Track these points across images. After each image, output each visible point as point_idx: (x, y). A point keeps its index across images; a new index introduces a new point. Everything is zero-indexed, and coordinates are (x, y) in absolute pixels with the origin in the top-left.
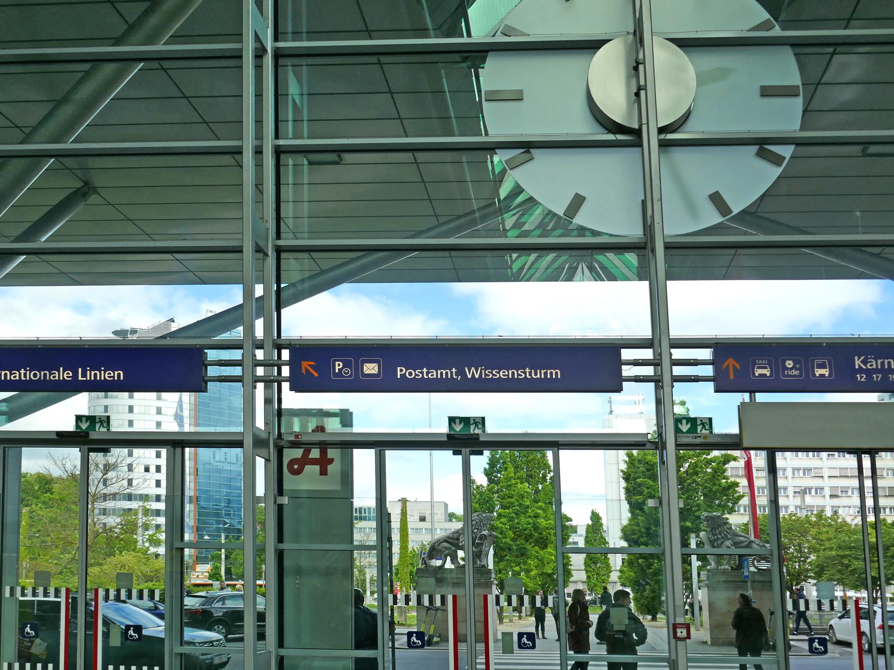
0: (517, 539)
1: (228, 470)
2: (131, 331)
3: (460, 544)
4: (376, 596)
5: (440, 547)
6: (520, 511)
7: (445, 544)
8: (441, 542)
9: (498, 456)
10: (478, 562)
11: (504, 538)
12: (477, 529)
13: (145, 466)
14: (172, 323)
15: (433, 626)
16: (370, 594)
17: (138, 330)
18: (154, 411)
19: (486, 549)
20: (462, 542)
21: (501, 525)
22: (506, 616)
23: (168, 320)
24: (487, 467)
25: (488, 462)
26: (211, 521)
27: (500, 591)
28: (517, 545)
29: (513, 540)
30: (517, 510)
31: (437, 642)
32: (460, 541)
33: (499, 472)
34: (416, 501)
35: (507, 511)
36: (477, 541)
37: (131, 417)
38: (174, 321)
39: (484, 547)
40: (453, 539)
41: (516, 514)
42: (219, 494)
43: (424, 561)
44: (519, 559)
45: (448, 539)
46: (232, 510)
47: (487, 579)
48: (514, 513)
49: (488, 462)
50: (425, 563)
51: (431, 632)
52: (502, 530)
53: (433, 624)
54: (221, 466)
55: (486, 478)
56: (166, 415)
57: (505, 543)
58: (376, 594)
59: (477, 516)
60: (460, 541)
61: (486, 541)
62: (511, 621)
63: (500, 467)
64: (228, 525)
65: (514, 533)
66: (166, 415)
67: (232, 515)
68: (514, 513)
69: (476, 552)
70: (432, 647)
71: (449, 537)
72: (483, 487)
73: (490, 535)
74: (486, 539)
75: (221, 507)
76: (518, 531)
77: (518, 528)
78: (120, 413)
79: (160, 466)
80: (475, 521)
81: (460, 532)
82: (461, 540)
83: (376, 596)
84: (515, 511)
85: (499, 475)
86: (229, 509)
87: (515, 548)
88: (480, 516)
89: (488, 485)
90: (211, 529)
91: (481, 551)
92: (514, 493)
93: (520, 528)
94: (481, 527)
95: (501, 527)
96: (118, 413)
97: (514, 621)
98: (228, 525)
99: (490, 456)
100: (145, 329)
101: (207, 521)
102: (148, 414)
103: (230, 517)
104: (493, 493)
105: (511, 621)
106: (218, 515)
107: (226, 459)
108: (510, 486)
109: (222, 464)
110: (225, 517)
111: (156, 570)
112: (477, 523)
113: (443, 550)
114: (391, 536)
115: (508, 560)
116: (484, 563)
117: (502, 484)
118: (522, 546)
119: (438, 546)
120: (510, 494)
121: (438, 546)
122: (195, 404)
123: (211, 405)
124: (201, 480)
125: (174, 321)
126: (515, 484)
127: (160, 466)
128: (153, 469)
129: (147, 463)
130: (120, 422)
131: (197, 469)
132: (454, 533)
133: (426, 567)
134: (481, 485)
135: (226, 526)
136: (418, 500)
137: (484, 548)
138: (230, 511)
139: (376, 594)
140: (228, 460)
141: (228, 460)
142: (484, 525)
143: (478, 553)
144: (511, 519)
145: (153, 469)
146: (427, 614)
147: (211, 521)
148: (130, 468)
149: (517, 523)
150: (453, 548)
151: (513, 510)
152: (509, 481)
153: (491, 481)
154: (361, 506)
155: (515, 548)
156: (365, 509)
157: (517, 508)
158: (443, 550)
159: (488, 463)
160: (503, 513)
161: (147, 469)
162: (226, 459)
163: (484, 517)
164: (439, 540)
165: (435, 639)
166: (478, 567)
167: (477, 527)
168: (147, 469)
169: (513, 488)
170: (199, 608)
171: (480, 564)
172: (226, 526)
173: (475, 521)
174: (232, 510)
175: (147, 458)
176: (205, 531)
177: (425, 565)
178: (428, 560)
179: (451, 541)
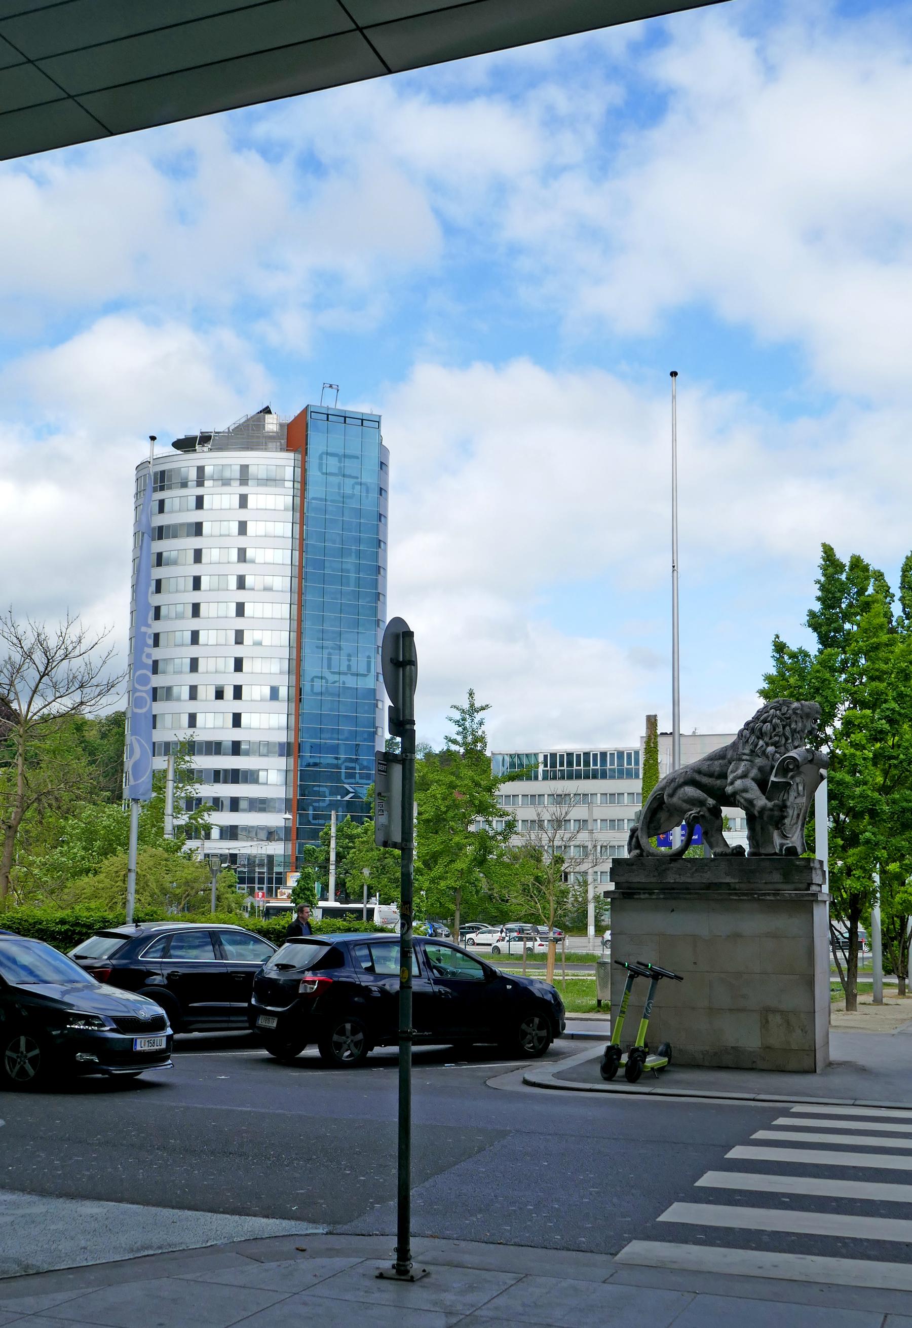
0: (893, 787)
1: (354, 688)
2: (200, 437)
3: (729, 789)
4: (608, 935)
5: (675, 800)
6: (900, 714)
7: (690, 791)
8: (681, 786)
9: (843, 577)
10: (777, 840)
11: (858, 783)
12: (775, 744)
13: (216, 688)
14: (267, 416)
15: (644, 1024)
16: (596, 931)
17: (212, 434)
18: (233, 582)
19: (798, 800)
20: (732, 783)
21: (852, 751)
22: (865, 984)
23: (261, 412)
24: (817, 607)
25: (819, 594)
26: (322, 789)
27: (848, 924)
28: (894, 802)
29: (884, 790)
30: (893, 710)
31: (661, 1070)
32: (729, 780)
33: (847, 617)
34: (694, 735)
35: (868, 712)
36: (773, 778)
37: (195, 597)
38: (269, 412)
39: (793, 794)
40: (710, 775)
41: (891, 721)
42: (335, 736)
43: (634, 840)
44: (898, 838)
45: (698, 777)
46: (358, 767)
47: (800, 886)
48: (886, 718)
49: (819, 594)
50: (638, 846)
51: (640, 1043)
52: (857, 765)
53: (645, 1017)
54: (341, 682)
55: (815, 634)
56: (253, 589)
57: (861, 796)
58: (608, 932)
59: (776, 708)
60: (729, 780)
61: (798, 779)
62: (878, 1001)
63: (850, 605)
64: (351, 795)
65: (886, 773)
66: (253, 589)
67: (357, 776)
68: (886, 718)
69: (771, 810)
70: (643, 1084)
71: (699, 772)
72: (806, 655)
73: (811, 761)
74: (799, 773)
75: (340, 762)
76: (896, 766)
77: (896, 758)
78: (180, 592)
79: (241, 686)
80: (771, 722)
81: (730, 754)
82: (730, 777)
83: (608, 935)
84: (888, 713)
85: (847, 626)
86: (353, 765)
87: (886, 808)
88: (784, 709)
89: (821, 652)
90: (321, 804)
91: (783, 807)
92: (884, 667)
93: (902, 756)
94: (787, 739)
95: (853, 755)
96: (177, 591)
97: (885, 1000)
98: (351, 795)
99: (823, 579)
100: (223, 432)
101: (315, 789)
102: (223, 590)
103: (352, 781)
104: (833, 670)
105: (878, 1001)
106: (336, 777)
107: (349, 667)
108: (876, 648)
109: (343, 678)
110: (346, 781)
111: (187, 883)
112: (774, 727)
113: (685, 806)
114: (412, 714)
115: (868, 841)
116: (795, 840)
117: (854, 644)
118: (905, 804)
119: (671, 796)
120: (877, 670)
121: (671, 796)
122: (301, 567)
123: (327, 564)
124: (306, 708)
125: (269, 412)
126: (887, 645)
127: (241, 686)
128: (229, 693)
129: (220, 682)
130: (180, 608)
131: (301, 689)
132: (712, 758)
133: (641, 855)
134: (801, 651)
135: (347, 798)
136: (698, 733)
137: (791, 798)
138: (354, 769)
139: (608, 932)
140: (354, 670)
141: (354, 670)
142: (794, 731)
143: (776, 813)
144: (878, 736)
145: (229, 693)
146: (629, 988)
147: (322, 789)
148: (193, 693)
149: (893, 747)
150: (711, 802)
151: (882, 711)
152: (875, 635)
153: (825, 640)
154: (587, 750)
155: (886, 808)
156: (595, 755)
157: (893, 705)
158: (685, 806)
159: (818, 599)
160: (857, 718)
161: (219, 695)
162: (349, 667)
163: (795, 709)
164: (673, 780)
165: (652, 1061)
166: (775, 854)
167: (776, 739)
168: (219, 695)
169: (882, 654)
170: (108, 962)
171: (782, 845)
172: (347, 798)
173: (771, 722)
174: (358, 767)
175: (220, 672)
176: (311, 808)
177: (638, 851)
178: (645, 837)
179: (705, 780)
